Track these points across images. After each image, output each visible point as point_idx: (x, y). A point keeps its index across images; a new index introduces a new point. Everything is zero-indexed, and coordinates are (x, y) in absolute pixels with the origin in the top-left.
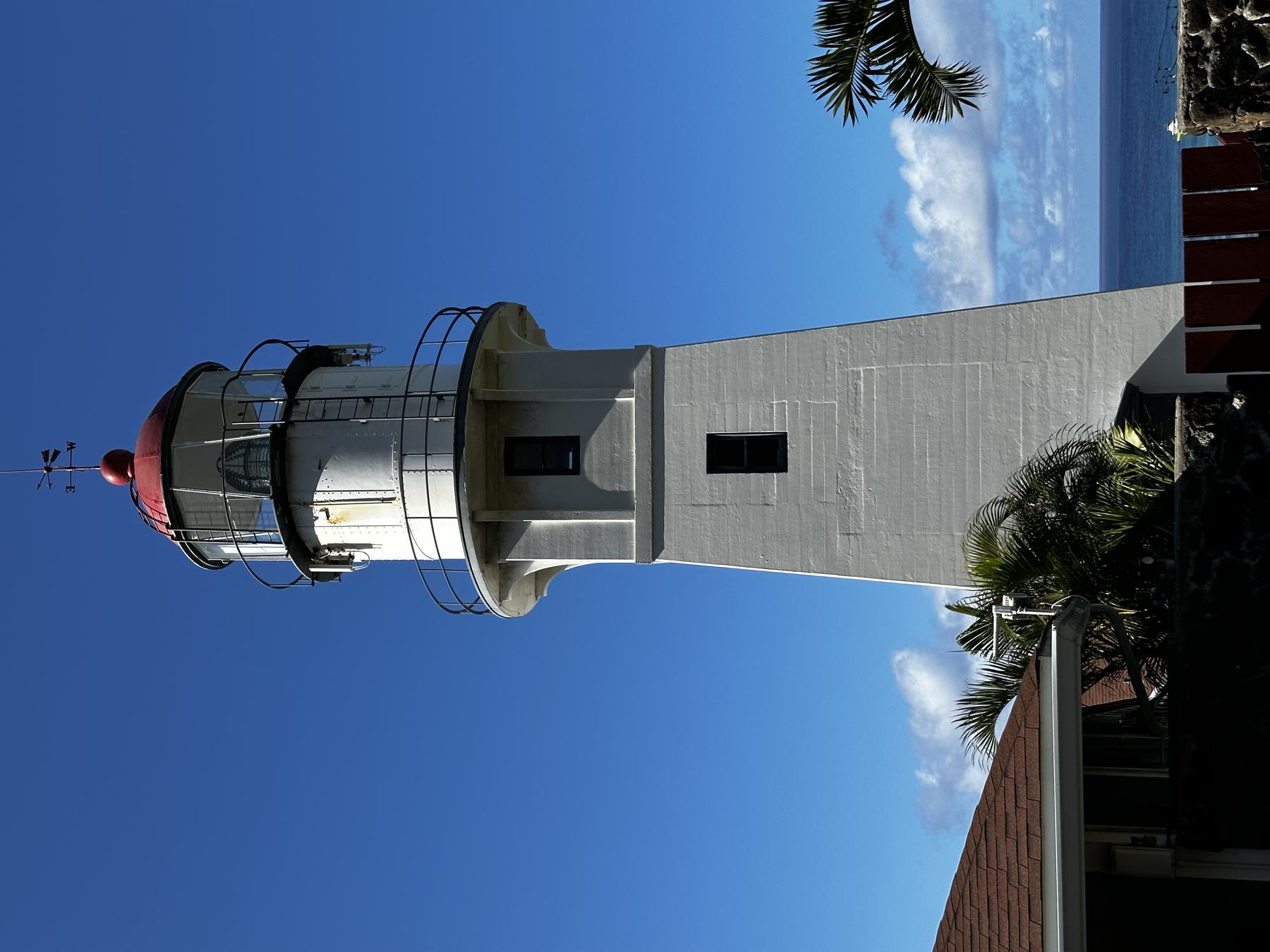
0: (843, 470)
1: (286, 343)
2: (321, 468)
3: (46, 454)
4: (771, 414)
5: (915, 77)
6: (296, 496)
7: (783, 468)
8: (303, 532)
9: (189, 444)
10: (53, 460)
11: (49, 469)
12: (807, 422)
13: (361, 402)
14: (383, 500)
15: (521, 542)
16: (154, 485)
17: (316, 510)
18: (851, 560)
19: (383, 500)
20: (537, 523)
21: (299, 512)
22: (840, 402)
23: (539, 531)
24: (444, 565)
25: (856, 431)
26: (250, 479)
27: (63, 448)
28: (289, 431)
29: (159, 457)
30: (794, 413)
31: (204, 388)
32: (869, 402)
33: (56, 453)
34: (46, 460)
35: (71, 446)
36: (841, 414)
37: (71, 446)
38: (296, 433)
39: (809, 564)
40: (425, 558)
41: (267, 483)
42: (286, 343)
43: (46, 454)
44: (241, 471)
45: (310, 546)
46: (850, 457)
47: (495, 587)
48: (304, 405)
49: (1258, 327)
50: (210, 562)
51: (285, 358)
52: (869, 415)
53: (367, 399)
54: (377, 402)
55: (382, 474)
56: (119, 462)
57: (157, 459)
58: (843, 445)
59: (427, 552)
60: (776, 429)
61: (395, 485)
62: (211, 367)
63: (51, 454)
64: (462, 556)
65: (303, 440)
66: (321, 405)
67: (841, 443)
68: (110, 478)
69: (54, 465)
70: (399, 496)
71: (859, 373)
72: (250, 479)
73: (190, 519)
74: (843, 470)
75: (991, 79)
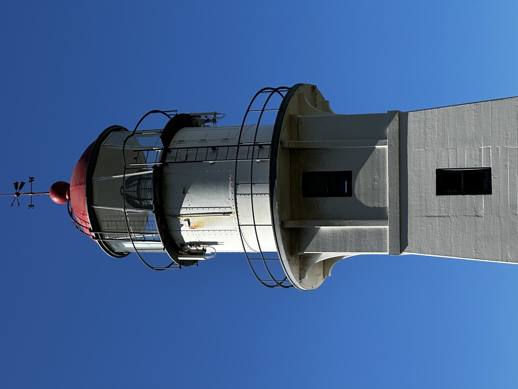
2: (185, 193)
3: (16, 184)
9: (103, 178)
11: (18, 194)
14: (224, 214)
15: (314, 241)
17: (182, 220)
19: (224, 214)
27: (27, 181)
29: (85, 186)
30: (496, 155)
34: (16, 188)
43: (16, 184)
56: (61, 189)
57: (84, 187)
68: (56, 200)
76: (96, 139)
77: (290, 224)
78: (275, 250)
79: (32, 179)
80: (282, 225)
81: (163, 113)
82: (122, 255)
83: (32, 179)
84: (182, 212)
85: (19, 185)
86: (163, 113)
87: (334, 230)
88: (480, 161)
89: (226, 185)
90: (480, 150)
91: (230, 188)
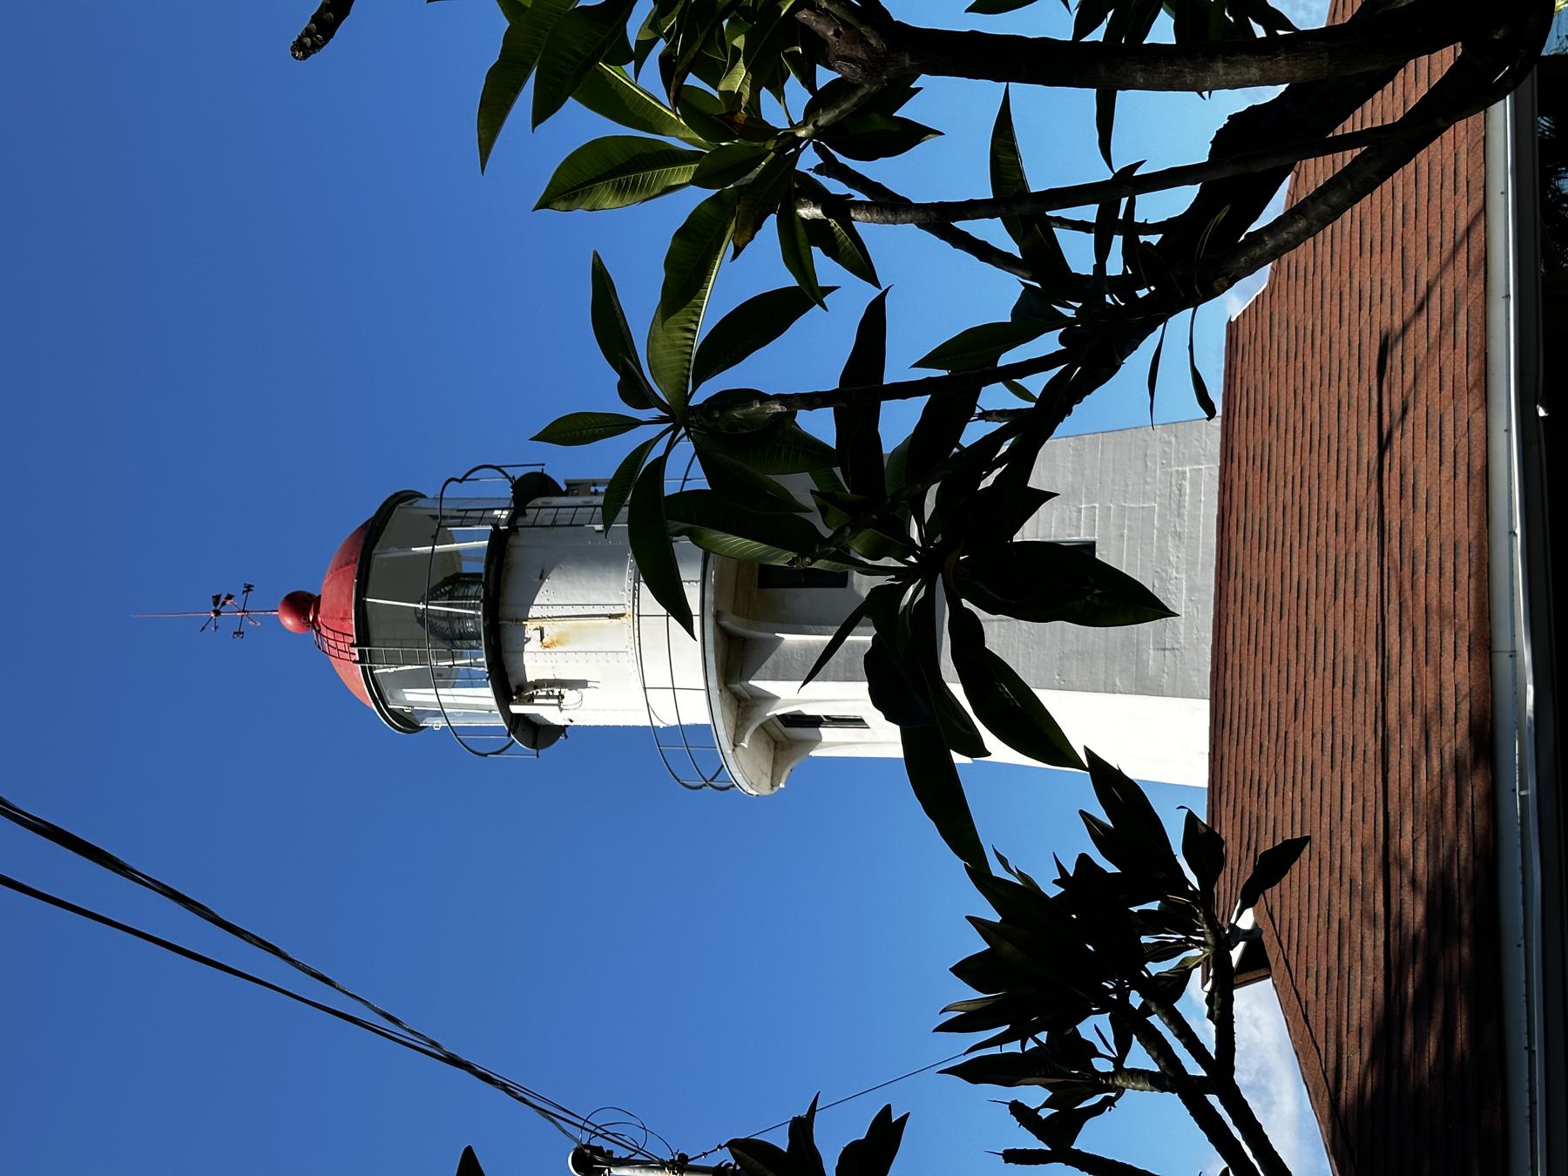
0: (1161, 579)
2: (542, 577)
3: (217, 599)
4: (1079, 519)
6: (508, 610)
8: (509, 659)
9: (394, 553)
11: (217, 613)
12: (1121, 527)
14: (611, 616)
15: (769, 662)
16: (344, 599)
17: (530, 630)
18: (1165, 679)
19: (611, 616)
20: (789, 638)
21: (509, 632)
22: (1160, 504)
23: (792, 650)
24: (684, 733)
25: (1179, 535)
27: (238, 591)
28: (512, 540)
29: (356, 567)
30: (1106, 517)
32: (1196, 503)
34: (216, 604)
36: (1162, 517)
39: (1114, 685)
43: (217, 599)
45: (513, 683)
46: (1170, 563)
47: (732, 725)
49: (1121, 217)
50: (389, 710)
52: (1194, 518)
55: (613, 585)
56: (302, 604)
57: (354, 568)
58: (1162, 552)
59: (666, 718)
60: (1084, 536)
61: (627, 598)
64: (707, 721)
65: (525, 548)
67: (1159, 549)
68: (289, 622)
70: (629, 611)
71: (1184, 473)
73: (375, 632)
74: (1161, 579)
76: (372, 514)
77: (733, 623)
78: (793, 282)
79: (249, 588)
80: (717, 616)
81: (498, 468)
82: (407, 722)
83: (249, 588)
84: (533, 612)
85: (222, 599)
86: (498, 468)
87: (808, 643)
88: (1078, 527)
89: (621, 564)
90: (1079, 511)
91: (628, 570)
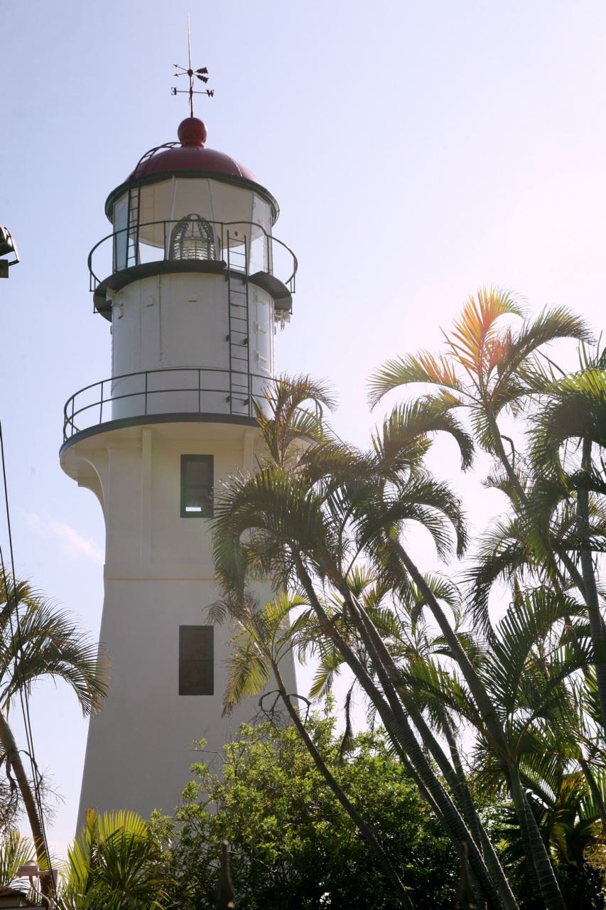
1: (294, 276)
5: (504, 672)
7: (212, 694)
10: (199, 77)
13: (244, 337)
26: (181, 242)
31: (260, 206)
33: (205, 80)
34: (199, 71)
35: (210, 93)
37: (210, 93)
38: (220, 278)
40: (369, 698)
41: (178, 257)
42: (294, 276)
43: (204, 71)
44: (188, 234)
48: (243, 289)
51: (281, 273)
53: (246, 341)
54: (244, 350)
62: (274, 213)
63: (204, 75)
66: (243, 303)
69: (194, 77)
72: (181, 242)
75: (236, 230)
